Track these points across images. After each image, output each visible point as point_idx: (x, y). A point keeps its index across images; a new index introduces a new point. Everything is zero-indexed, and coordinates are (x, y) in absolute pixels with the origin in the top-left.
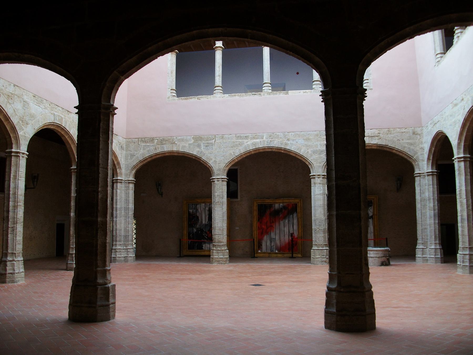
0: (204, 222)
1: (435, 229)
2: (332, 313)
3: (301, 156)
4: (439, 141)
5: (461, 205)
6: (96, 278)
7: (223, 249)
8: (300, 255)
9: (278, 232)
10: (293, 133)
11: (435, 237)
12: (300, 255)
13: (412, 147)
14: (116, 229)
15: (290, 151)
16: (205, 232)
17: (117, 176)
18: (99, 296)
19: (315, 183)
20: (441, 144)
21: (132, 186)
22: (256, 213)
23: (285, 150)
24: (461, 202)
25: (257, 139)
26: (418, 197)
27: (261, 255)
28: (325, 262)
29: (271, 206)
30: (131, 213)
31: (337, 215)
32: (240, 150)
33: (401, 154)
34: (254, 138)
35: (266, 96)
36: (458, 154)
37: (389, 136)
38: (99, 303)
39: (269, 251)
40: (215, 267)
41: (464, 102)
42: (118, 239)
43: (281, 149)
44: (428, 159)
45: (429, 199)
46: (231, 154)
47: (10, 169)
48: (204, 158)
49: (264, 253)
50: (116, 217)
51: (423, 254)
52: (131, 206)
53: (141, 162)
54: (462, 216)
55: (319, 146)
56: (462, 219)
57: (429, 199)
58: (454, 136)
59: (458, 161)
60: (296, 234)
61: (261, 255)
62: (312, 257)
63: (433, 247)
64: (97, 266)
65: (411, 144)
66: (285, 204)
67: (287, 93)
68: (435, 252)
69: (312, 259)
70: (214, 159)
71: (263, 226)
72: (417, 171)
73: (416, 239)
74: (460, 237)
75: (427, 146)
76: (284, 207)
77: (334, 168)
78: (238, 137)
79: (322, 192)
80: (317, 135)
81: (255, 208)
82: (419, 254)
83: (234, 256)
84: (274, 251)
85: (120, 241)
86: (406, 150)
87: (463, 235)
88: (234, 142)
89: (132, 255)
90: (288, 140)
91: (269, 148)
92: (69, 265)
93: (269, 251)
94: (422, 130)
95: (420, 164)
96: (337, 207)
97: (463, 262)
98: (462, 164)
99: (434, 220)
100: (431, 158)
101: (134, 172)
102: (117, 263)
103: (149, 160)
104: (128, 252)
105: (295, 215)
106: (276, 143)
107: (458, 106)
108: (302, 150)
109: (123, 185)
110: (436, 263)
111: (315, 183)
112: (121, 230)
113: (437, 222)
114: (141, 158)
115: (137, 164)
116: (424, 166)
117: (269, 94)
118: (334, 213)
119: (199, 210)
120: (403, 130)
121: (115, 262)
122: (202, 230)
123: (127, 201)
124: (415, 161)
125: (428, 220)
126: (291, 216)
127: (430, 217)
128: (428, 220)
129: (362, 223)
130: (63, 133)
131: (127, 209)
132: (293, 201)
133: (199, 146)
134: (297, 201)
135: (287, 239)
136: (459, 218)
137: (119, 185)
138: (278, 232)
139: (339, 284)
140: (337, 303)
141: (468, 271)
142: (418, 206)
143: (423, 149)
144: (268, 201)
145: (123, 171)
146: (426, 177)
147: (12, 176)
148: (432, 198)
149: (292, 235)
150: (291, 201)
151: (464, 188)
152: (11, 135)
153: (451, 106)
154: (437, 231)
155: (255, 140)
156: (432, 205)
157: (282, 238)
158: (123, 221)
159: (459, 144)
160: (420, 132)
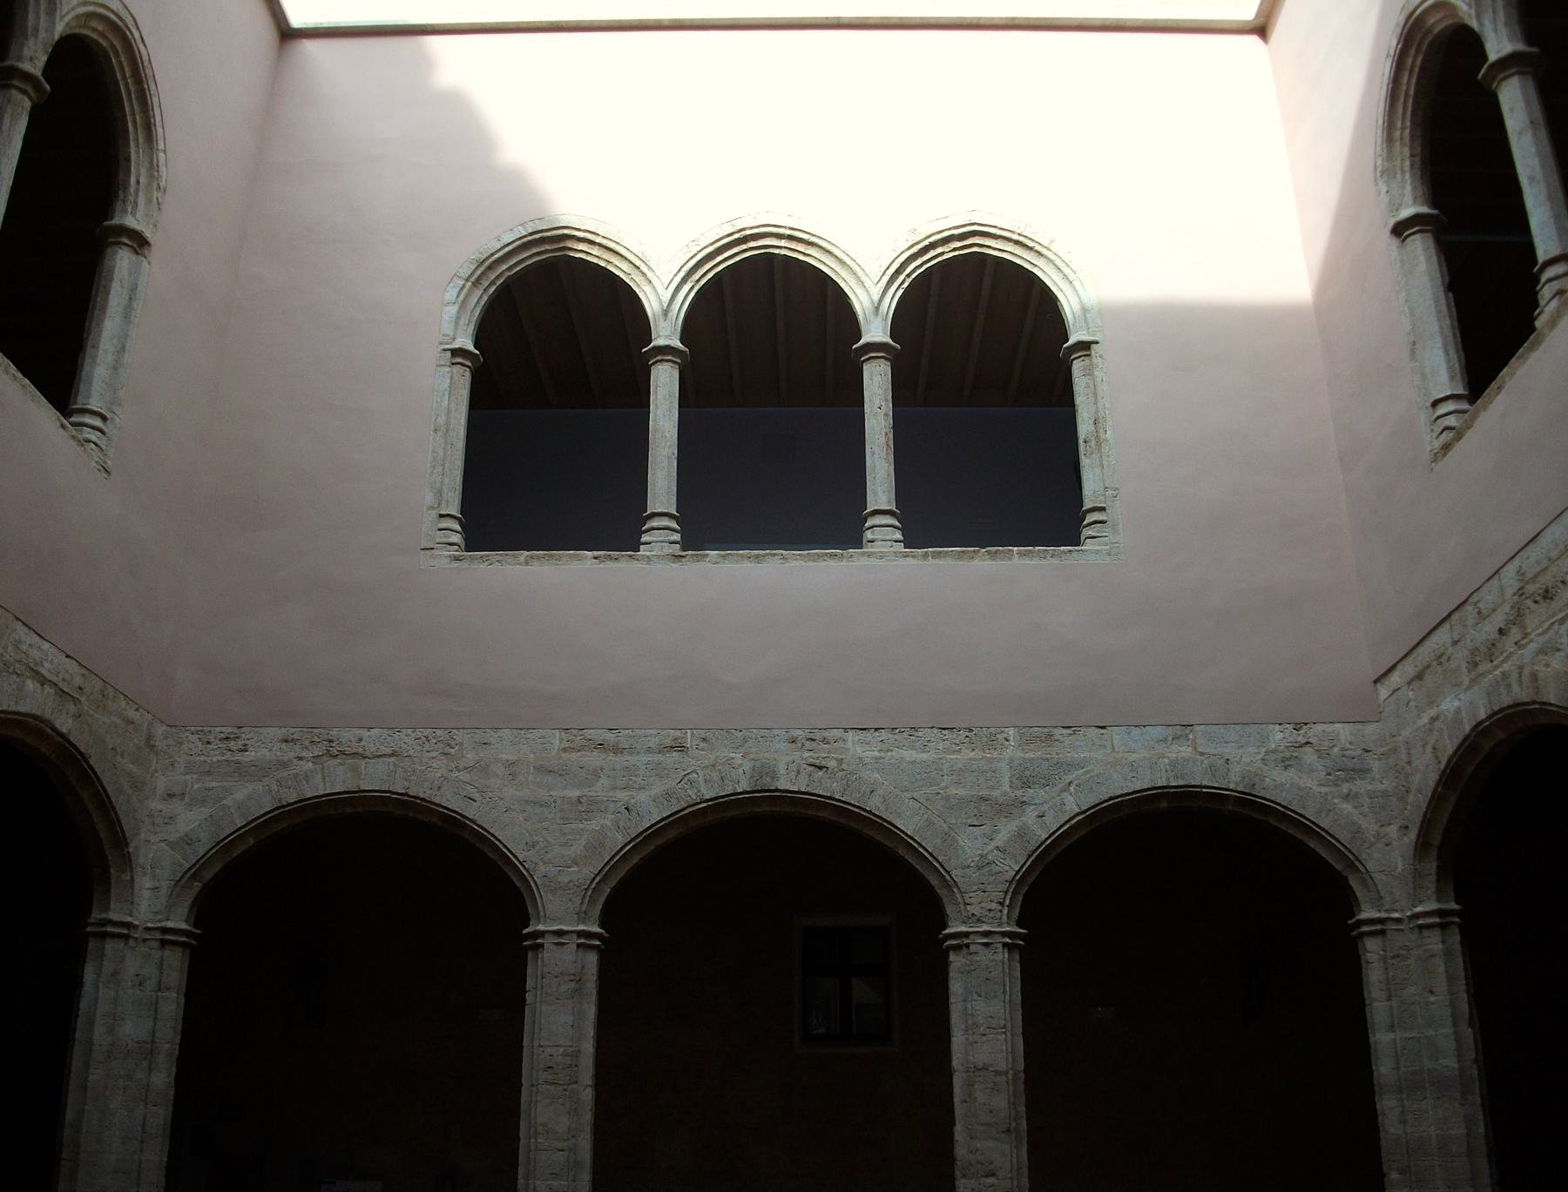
59: (579, 946)
100: (208, 875)
153: (557, 740)
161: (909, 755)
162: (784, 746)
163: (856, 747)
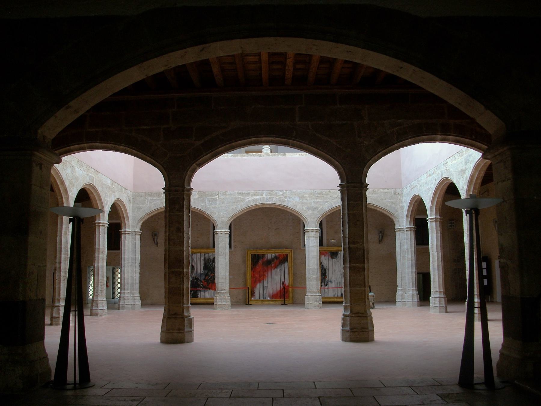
0: (199, 272)
1: (412, 278)
2: (347, 331)
3: (297, 212)
4: (416, 202)
5: (433, 258)
6: (183, 312)
7: (226, 296)
8: (290, 302)
9: (270, 280)
10: (290, 192)
11: (413, 283)
12: (290, 302)
13: (393, 206)
14: (125, 278)
15: (286, 207)
16: (201, 281)
17: (125, 228)
18: (186, 325)
19: (309, 237)
20: (418, 205)
21: (138, 237)
22: (249, 263)
23: (282, 206)
24: (433, 255)
25: (257, 196)
26: (398, 249)
27: (254, 302)
28: (318, 306)
29: (263, 256)
30: (138, 263)
31: (350, 267)
32: (241, 205)
33: (383, 212)
34: (254, 195)
35: (266, 157)
36: (431, 216)
37: (374, 195)
38: (186, 330)
39: (262, 299)
40: (218, 311)
41: (435, 175)
42: (126, 287)
43: (278, 205)
44: (407, 216)
45: (408, 251)
46: (233, 209)
47: (62, 226)
48: (208, 212)
49: (257, 300)
50: (124, 267)
51: (402, 299)
52: (138, 256)
53: (147, 214)
54: (433, 266)
55: (313, 204)
56: (433, 268)
57: (408, 251)
58: (428, 201)
60: (287, 283)
61: (254, 302)
62: (306, 302)
63: (411, 293)
64: (183, 304)
65: (393, 203)
66: (277, 254)
67: (285, 155)
68: (413, 297)
69: (306, 304)
70: (217, 214)
71: (256, 275)
72: (397, 227)
73: (396, 286)
74: (432, 283)
75: (406, 205)
76: (276, 257)
77: (347, 236)
78: (240, 194)
79: (315, 244)
80: (311, 194)
81: (249, 258)
82: (398, 299)
83: (235, 304)
84: (267, 299)
85: (128, 289)
86: (388, 208)
87: (434, 282)
88: (236, 198)
89: (138, 302)
90: (285, 197)
91: (268, 204)
92: (94, 311)
93: (262, 299)
94: (402, 191)
95: (400, 220)
96: (350, 261)
97: (434, 303)
98: (434, 223)
99: (412, 269)
100: (410, 216)
101: (140, 224)
102: (125, 310)
103: (155, 213)
104: (135, 299)
105: (286, 264)
106: (274, 200)
107: (431, 177)
108: (298, 207)
109: (130, 236)
110: (413, 306)
111: (309, 237)
112: (128, 279)
113: (414, 271)
114: (148, 211)
115: (144, 217)
116: (403, 224)
117: (268, 155)
118: (348, 265)
119: (195, 260)
120: (386, 191)
121: (123, 309)
122: (197, 279)
123: (134, 251)
124: (396, 217)
125: (407, 269)
126: (283, 265)
127: (409, 267)
128: (407, 269)
129: (366, 272)
130: (93, 191)
131: (134, 259)
132: (284, 251)
133: (203, 201)
134: (287, 251)
135: (278, 287)
136: (431, 268)
137: (127, 236)
138: (270, 280)
139: (351, 312)
140: (350, 324)
141: (438, 311)
142: (398, 257)
143: (402, 207)
144: (260, 252)
145: (131, 222)
146: (405, 232)
147: (63, 232)
148: (410, 250)
149: (283, 283)
150: (283, 251)
151: (435, 243)
152: (63, 197)
153: (425, 175)
154: (414, 279)
155: (255, 197)
156: (410, 256)
157: (274, 286)
158: (130, 271)
159: (432, 207)
160: (400, 193)
161: (454, 162)
162: (443, 166)
163: (450, 163)
